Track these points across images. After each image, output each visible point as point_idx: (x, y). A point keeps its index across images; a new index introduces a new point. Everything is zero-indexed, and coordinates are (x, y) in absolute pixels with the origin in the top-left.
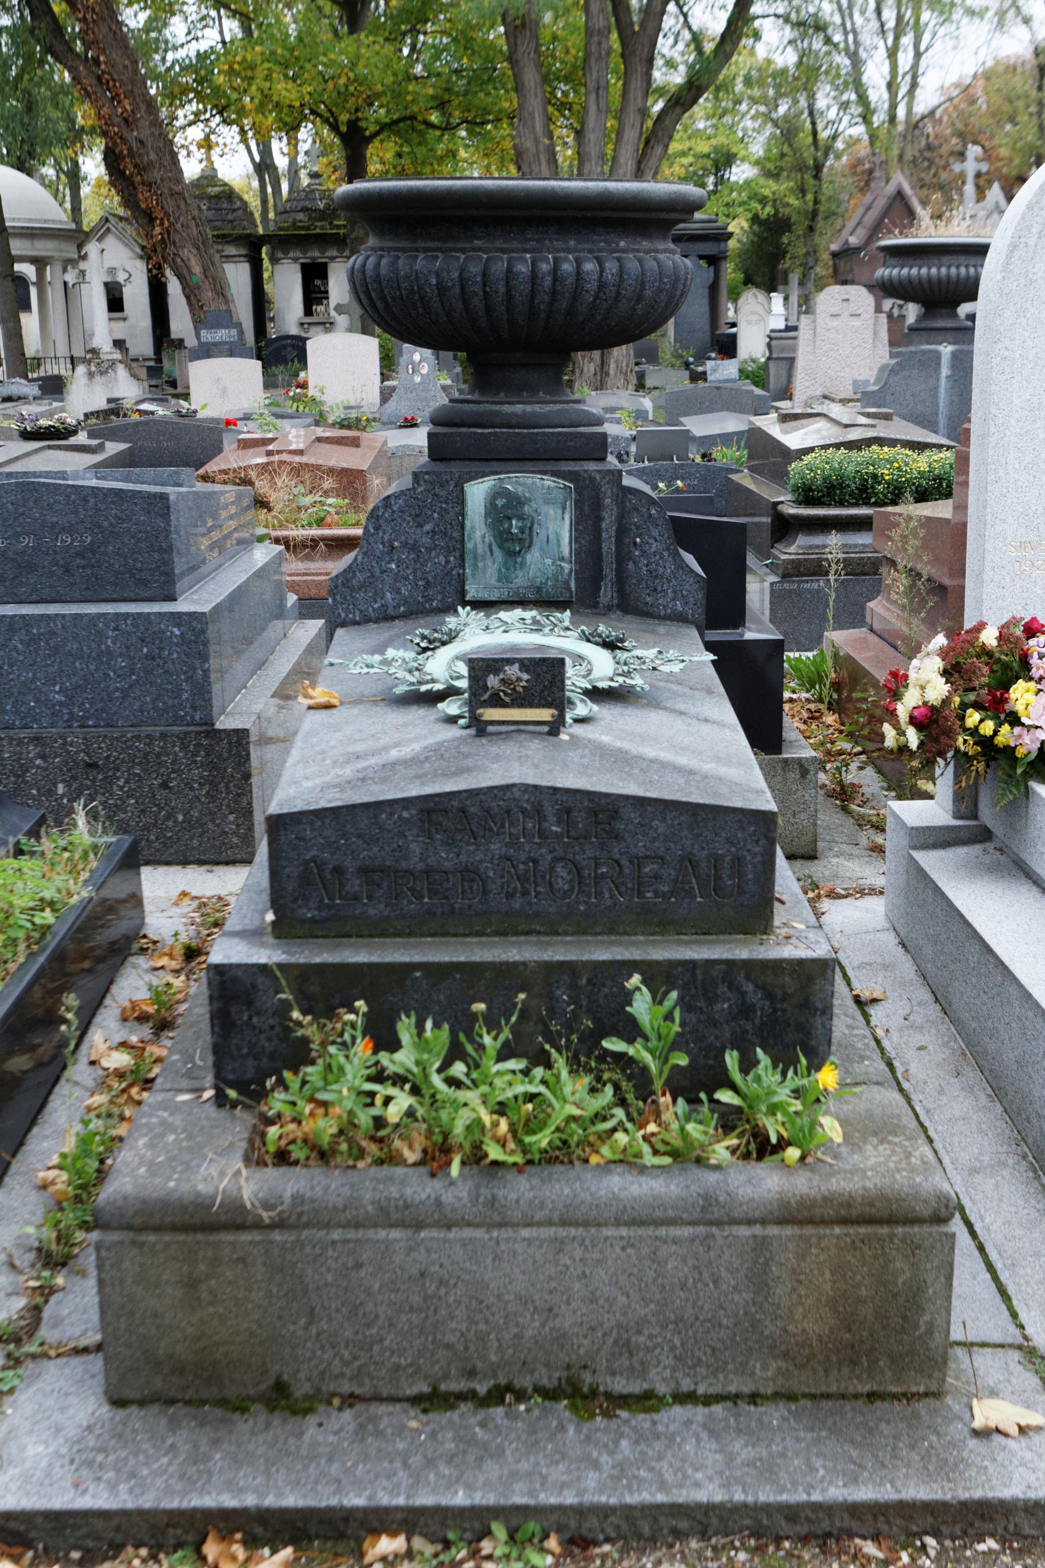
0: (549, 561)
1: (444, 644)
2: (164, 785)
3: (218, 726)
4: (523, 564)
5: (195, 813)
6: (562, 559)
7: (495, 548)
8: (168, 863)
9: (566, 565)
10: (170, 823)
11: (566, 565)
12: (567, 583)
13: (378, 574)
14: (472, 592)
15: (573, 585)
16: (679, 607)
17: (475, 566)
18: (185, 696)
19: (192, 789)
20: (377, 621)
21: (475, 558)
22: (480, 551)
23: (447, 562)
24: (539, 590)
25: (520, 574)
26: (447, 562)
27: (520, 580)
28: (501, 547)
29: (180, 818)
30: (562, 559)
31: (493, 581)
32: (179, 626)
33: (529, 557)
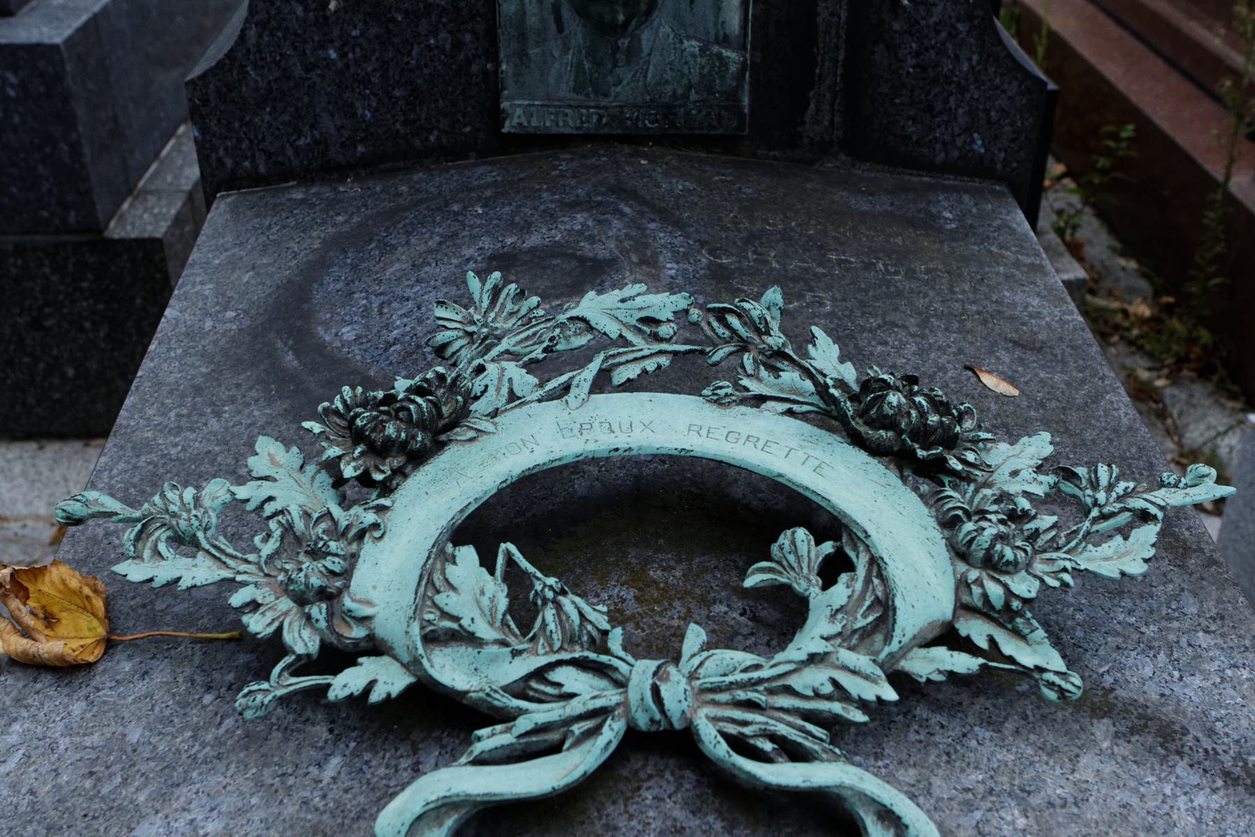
0: (692, 46)
1: (418, 458)
2: (36, 324)
3: (115, 231)
4: (632, 52)
5: (94, 366)
6: (725, 41)
7: (566, 13)
8: (62, 437)
9: (730, 54)
10: (56, 380)
11: (730, 54)
12: (733, 95)
13: (298, 71)
14: (518, 113)
15: (746, 101)
16: (978, 145)
17: (522, 55)
18: (45, 186)
19: (81, 329)
20: (306, 177)
21: (522, 37)
22: (532, 21)
23: (458, 45)
24: (668, 111)
25: (626, 74)
26: (458, 45)
27: (625, 87)
28: (581, 12)
29: (70, 372)
30: (725, 41)
31: (565, 91)
32: (15, 68)
33: (646, 37)
